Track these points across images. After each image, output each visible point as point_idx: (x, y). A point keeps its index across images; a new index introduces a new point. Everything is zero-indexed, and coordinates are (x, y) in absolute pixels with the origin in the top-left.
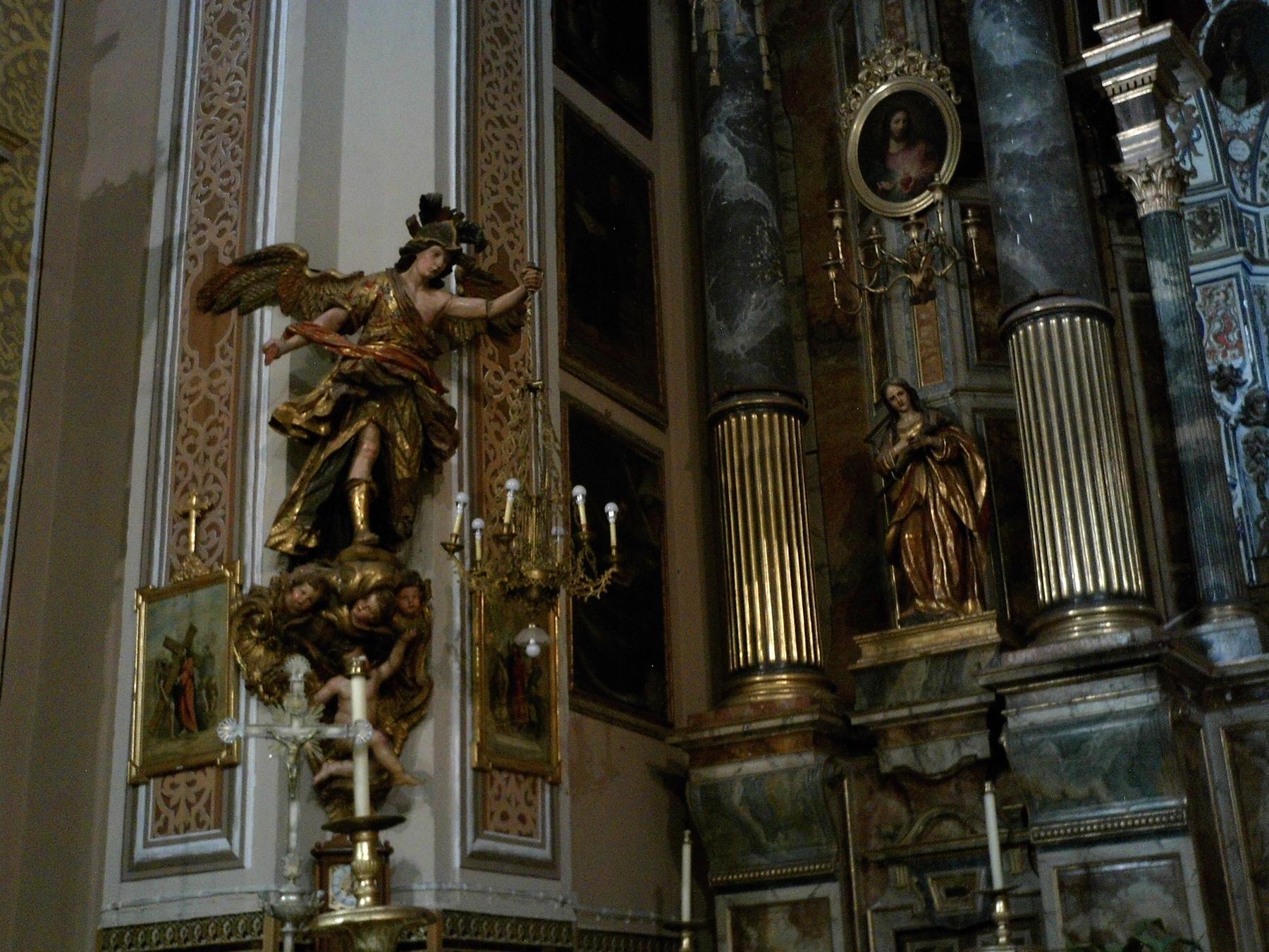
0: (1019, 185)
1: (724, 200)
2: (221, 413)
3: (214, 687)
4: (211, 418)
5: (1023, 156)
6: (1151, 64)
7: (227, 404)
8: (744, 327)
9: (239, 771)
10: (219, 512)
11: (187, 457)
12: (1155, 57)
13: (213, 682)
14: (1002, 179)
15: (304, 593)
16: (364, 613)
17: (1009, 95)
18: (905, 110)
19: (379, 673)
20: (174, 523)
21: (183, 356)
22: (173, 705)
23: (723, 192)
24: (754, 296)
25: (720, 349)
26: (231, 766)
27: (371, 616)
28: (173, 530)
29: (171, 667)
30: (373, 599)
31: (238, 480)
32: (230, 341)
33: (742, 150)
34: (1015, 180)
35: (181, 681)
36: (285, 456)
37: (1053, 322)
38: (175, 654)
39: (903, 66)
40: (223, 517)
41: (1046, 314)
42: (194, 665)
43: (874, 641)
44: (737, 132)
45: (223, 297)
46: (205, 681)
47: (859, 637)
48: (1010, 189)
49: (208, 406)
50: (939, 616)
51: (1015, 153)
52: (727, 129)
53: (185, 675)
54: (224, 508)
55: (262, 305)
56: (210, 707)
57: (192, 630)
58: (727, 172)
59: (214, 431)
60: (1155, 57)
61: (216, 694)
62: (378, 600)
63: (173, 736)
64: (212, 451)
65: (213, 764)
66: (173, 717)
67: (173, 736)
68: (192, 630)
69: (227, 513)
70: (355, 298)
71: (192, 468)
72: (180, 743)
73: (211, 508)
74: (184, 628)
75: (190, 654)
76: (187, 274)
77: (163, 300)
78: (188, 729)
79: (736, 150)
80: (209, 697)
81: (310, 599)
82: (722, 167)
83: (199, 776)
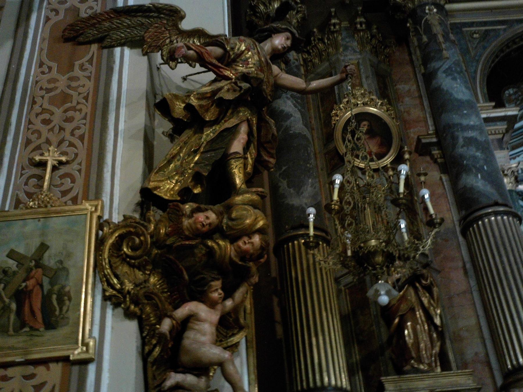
0: (476, 151)
1: (291, 131)
2: (78, 103)
3: (68, 294)
4: (69, 105)
5: (476, 139)
6: (504, 125)
7: (86, 98)
8: (306, 194)
9: (92, 368)
10: (75, 166)
11: (38, 125)
12: (506, 123)
13: (67, 289)
14: (465, 148)
15: (207, 218)
16: (247, 247)
17: (465, 112)
18: (368, 121)
19: (224, 306)
20: (23, 169)
21: (41, 64)
22: (14, 306)
23: (290, 127)
24: (310, 180)
25: (291, 203)
26: (84, 363)
27: (252, 251)
28: (22, 175)
29: (15, 273)
30: (256, 239)
31: (96, 145)
32: (90, 61)
33: (299, 110)
34: (474, 149)
35: (26, 287)
36: (143, 139)
37: (499, 218)
38: (20, 264)
39: (368, 101)
40: (80, 171)
41: (496, 214)
42: (44, 275)
43: (394, 381)
44: (296, 102)
45: (92, 33)
46: (56, 288)
47: (384, 378)
48: (472, 153)
49: (65, 98)
50: (422, 372)
51: (471, 137)
52: (291, 99)
53: (31, 283)
54: (80, 164)
55: (122, 45)
56: (61, 309)
57: (43, 247)
58: (292, 118)
59: (70, 114)
60: (506, 123)
61: (70, 299)
62: (260, 239)
63: (11, 332)
64: (69, 127)
65: (65, 359)
66: (13, 317)
67: (11, 332)
68: (43, 247)
69: (83, 167)
70: (232, 44)
71: (45, 134)
72: (21, 338)
73: (67, 162)
74: (36, 243)
75: (38, 265)
76: (47, 19)
77: (21, 31)
78: (31, 328)
79: (297, 109)
80: (61, 302)
81: (210, 224)
82: (288, 116)
83: (41, 370)
